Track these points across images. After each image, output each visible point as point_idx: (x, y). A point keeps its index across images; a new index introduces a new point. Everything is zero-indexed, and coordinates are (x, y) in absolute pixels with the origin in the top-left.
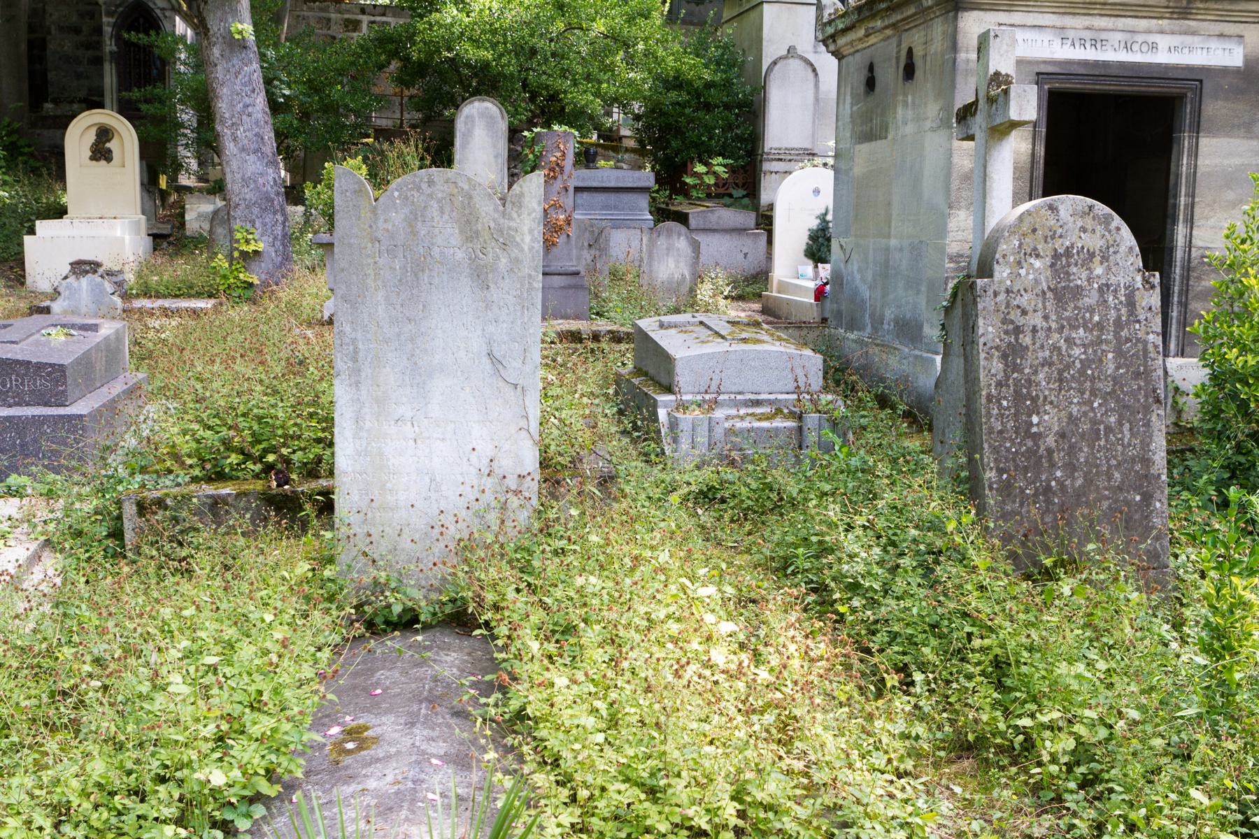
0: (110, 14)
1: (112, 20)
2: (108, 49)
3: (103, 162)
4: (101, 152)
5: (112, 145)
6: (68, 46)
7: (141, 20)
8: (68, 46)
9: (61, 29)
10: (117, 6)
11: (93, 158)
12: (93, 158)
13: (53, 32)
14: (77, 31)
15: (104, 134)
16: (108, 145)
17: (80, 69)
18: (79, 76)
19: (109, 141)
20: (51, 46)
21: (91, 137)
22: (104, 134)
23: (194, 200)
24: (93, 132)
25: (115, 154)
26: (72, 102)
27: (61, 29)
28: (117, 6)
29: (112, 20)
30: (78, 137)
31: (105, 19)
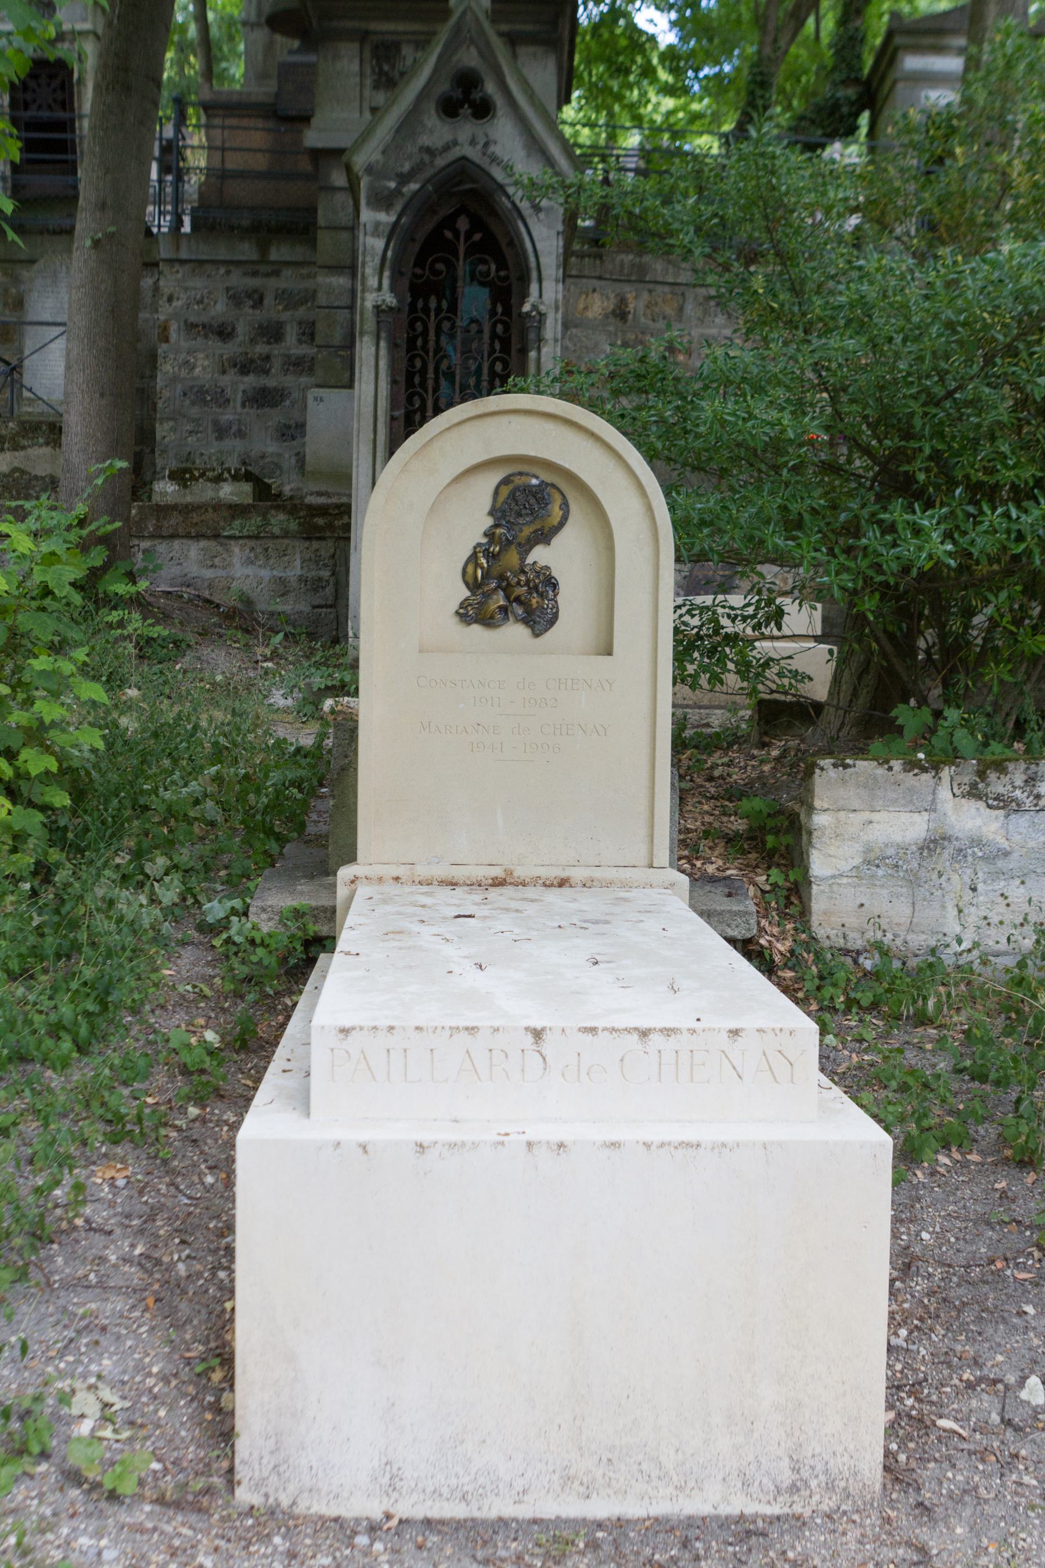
0: (382, 200)
1: (387, 218)
2: (370, 300)
3: (515, 632)
4: (506, 589)
5: (565, 557)
6: (203, 369)
7: (463, 224)
8: (203, 369)
9: (191, 327)
10: (404, 179)
11: (475, 613)
12: (475, 613)
13: (173, 336)
14: (224, 332)
15: (528, 504)
16: (539, 555)
17: (227, 416)
18: (221, 432)
19: (545, 536)
20: (167, 368)
21: (472, 520)
22: (528, 504)
23: (850, 795)
24: (482, 492)
25: (574, 599)
26: (219, 479)
27: (191, 327)
28: (404, 179)
29: (387, 218)
30: (415, 516)
31: (367, 215)
